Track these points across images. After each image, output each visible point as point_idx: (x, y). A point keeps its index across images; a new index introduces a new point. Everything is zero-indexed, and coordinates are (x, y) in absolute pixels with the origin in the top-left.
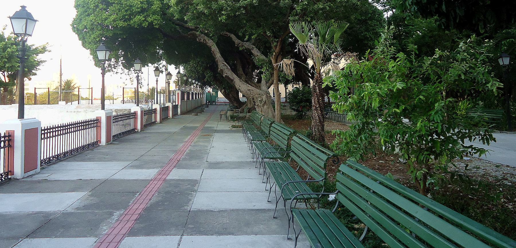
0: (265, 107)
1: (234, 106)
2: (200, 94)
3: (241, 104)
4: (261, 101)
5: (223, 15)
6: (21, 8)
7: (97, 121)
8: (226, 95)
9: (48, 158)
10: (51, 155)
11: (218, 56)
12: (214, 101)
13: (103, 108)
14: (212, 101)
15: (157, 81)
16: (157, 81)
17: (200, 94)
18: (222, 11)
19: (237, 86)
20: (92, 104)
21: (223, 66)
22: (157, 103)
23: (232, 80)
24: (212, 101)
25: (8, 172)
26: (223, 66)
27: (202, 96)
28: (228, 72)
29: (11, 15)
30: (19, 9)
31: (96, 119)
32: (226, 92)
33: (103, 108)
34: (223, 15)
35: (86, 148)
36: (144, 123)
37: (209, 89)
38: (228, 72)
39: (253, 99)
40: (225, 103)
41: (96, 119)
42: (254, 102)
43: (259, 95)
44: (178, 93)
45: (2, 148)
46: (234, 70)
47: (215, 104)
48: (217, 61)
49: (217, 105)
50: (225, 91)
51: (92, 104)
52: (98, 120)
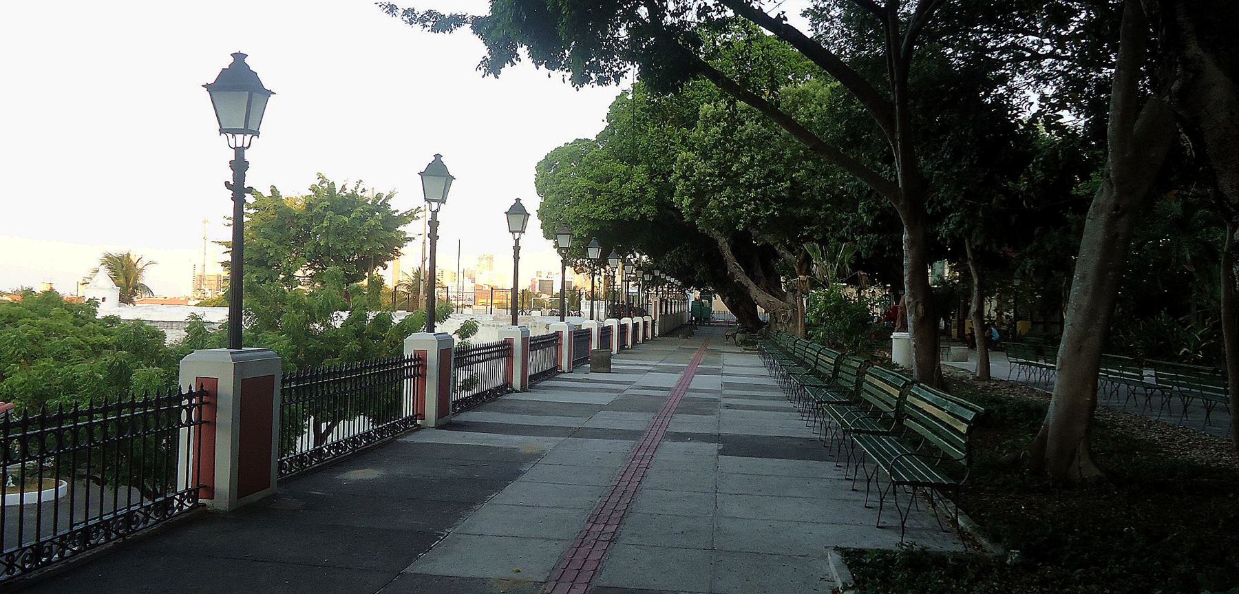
0: (791, 325)
1: (747, 327)
2: (673, 304)
3: (759, 324)
4: (785, 317)
5: (741, 223)
6: (434, 158)
7: (409, 363)
8: (733, 307)
9: (336, 443)
10: (356, 433)
11: (728, 253)
12: (708, 319)
13: (515, 322)
14: (702, 314)
15: (517, 248)
16: (517, 248)
17: (673, 304)
18: (741, 219)
19: (753, 297)
20: (491, 313)
21: (734, 266)
22: (592, 318)
23: (747, 288)
24: (702, 314)
25: (198, 489)
26: (734, 266)
27: (676, 306)
28: (741, 277)
29: (211, 81)
30: (227, 61)
31: (409, 358)
32: (732, 302)
33: (515, 322)
34: (741, 223)
35: (388, 434)
36: (531, 372)
37: (695, 295)
38: (741, 277)
39: (774, 313)
40: (729, 322)
41: (409, 358)
42: (776, 318)
43: (783, 308)
44: (656, 302)
45: (184, 426)
46: (749, 272)
47: (709, 325)
48: (726, 260)
49: (712, 326)
50: (731, 300)
51: (491, 313)
52: (509, 344)
